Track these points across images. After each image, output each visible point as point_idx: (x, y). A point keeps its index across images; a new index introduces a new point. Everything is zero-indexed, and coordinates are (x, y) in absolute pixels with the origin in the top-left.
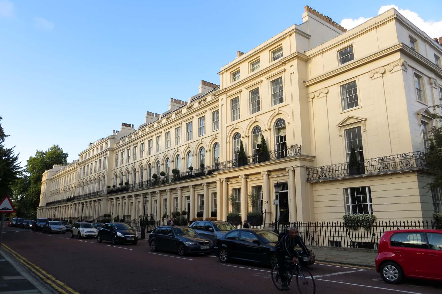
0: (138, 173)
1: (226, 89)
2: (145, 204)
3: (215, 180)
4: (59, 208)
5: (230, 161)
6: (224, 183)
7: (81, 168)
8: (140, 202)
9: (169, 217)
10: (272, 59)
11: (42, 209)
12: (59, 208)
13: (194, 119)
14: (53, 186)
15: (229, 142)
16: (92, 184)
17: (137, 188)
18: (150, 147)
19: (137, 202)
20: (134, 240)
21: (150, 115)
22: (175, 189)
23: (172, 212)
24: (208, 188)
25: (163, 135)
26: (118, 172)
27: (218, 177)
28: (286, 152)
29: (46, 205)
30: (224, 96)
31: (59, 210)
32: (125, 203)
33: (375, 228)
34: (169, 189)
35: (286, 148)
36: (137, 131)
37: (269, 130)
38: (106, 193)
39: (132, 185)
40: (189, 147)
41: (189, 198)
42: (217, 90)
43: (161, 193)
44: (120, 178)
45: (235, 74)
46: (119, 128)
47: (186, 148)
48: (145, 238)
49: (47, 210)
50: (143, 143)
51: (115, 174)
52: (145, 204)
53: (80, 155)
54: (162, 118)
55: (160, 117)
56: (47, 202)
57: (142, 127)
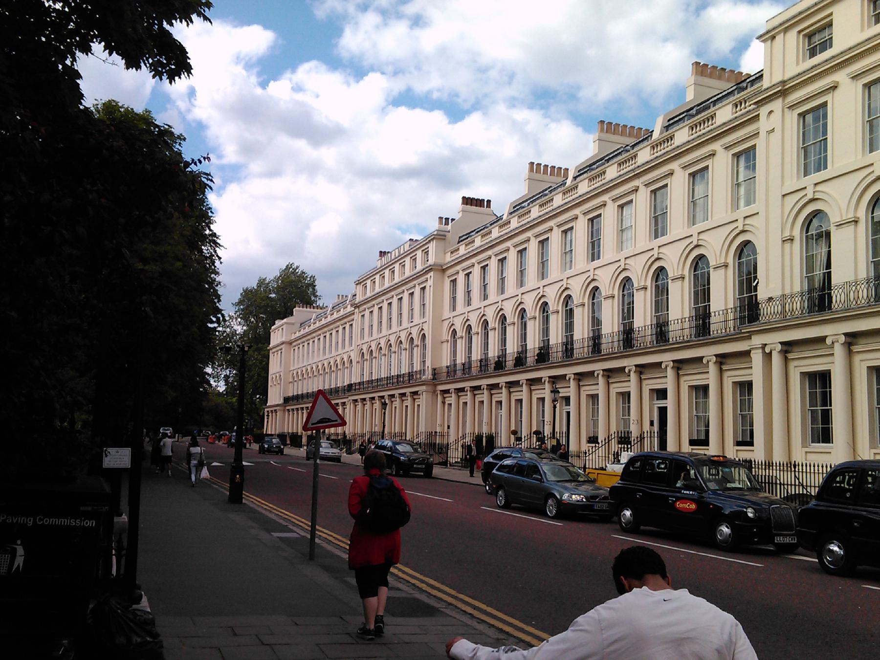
1: (783, 82)
3: (748, 348)
4: (408, 402)
5: (792, 296)
6: (776, 359)
7: (363, 316)
8: (543, 399)
10: (803, 51)
11: (785, 319)
13: (716, 158)
15: (792, 240)
16: (383, 358)
17: (475, 371)
18: (542, 258)
21: (538, 171)
24: (721, 369)
26: (458, 327)
27: (757, 340)
28: (830, 298)
29: (281, 401)
30: (777, 105)
32: (465, 403)
33: (817, 485)
34: (603, 370)
35: (830, 288)
36: (505, 217)
40: (661, 256)
41: (662, 394)
42: (749, 90)
45: (817, 38)
47: (619, 270)
50: (505, 258)
53: (358, 283)
54: (575, 178)
55: (571, 175)
57: (518, 208)
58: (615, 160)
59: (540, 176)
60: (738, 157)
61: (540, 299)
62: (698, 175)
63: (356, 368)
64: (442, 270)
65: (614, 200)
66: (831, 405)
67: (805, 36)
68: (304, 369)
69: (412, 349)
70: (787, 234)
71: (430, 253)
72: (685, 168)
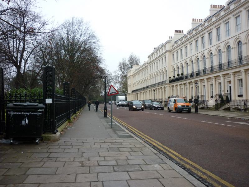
0: (215, 56)
2: (196, 88)
4: (160, 90)
8: (187, 88)
13: (231, 19)
18: (203, 42)
19: (185, 88)
22: (211, 78)
23: (217, 93)
25: (184, 48)
31: (146, 94)
38: (168, 82)
39: (186, 75)
40: (219, 46)
41: (230, 82)
43: (208, 80)
46: (173, 34)
48: (198, 112)
51: (210, 53)
52: (196, 88)
54: (204, 22)
55: (203, 21)
56: (132, 90)
57: (190, 32)
58: (215, 15)
59: (196, 22)
60: (226, 24)
61: (203, 54)
62: (227, 23)
63: (149, 81)
64: (170, 51)
65: (234, 16)
68: (145, 79)
72: (234, 16)
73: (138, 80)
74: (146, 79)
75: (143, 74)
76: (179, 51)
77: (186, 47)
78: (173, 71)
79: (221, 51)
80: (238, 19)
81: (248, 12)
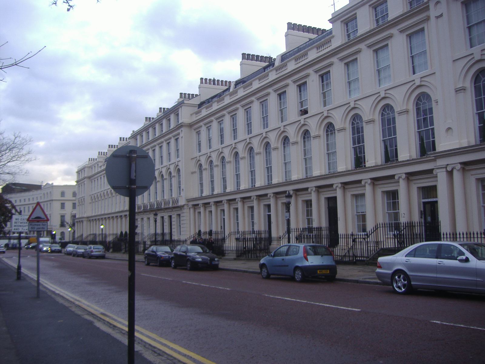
4: (119, 219)
9: (375, 232)
12: (95, 222)
14: (102, 183)
20: (328, 272)
37: (406, 113)
44: (176, 178)
49: (89, 223)
51: (168, 172)
61: (197, 162)
64: (190, 126)
65: (243, 106)
66: (399, 210)
67: (370, 6)
69: (171, 179)
70: (460, 85)
71: (171, 120)
73: (94, 193)
74: (82, 200)
75: (101, 181)
76: (165, 145)
77: (168, 143)
78: (197, 170)
79: (270, 146)
80: (382, 55)
81: (464, 6)
